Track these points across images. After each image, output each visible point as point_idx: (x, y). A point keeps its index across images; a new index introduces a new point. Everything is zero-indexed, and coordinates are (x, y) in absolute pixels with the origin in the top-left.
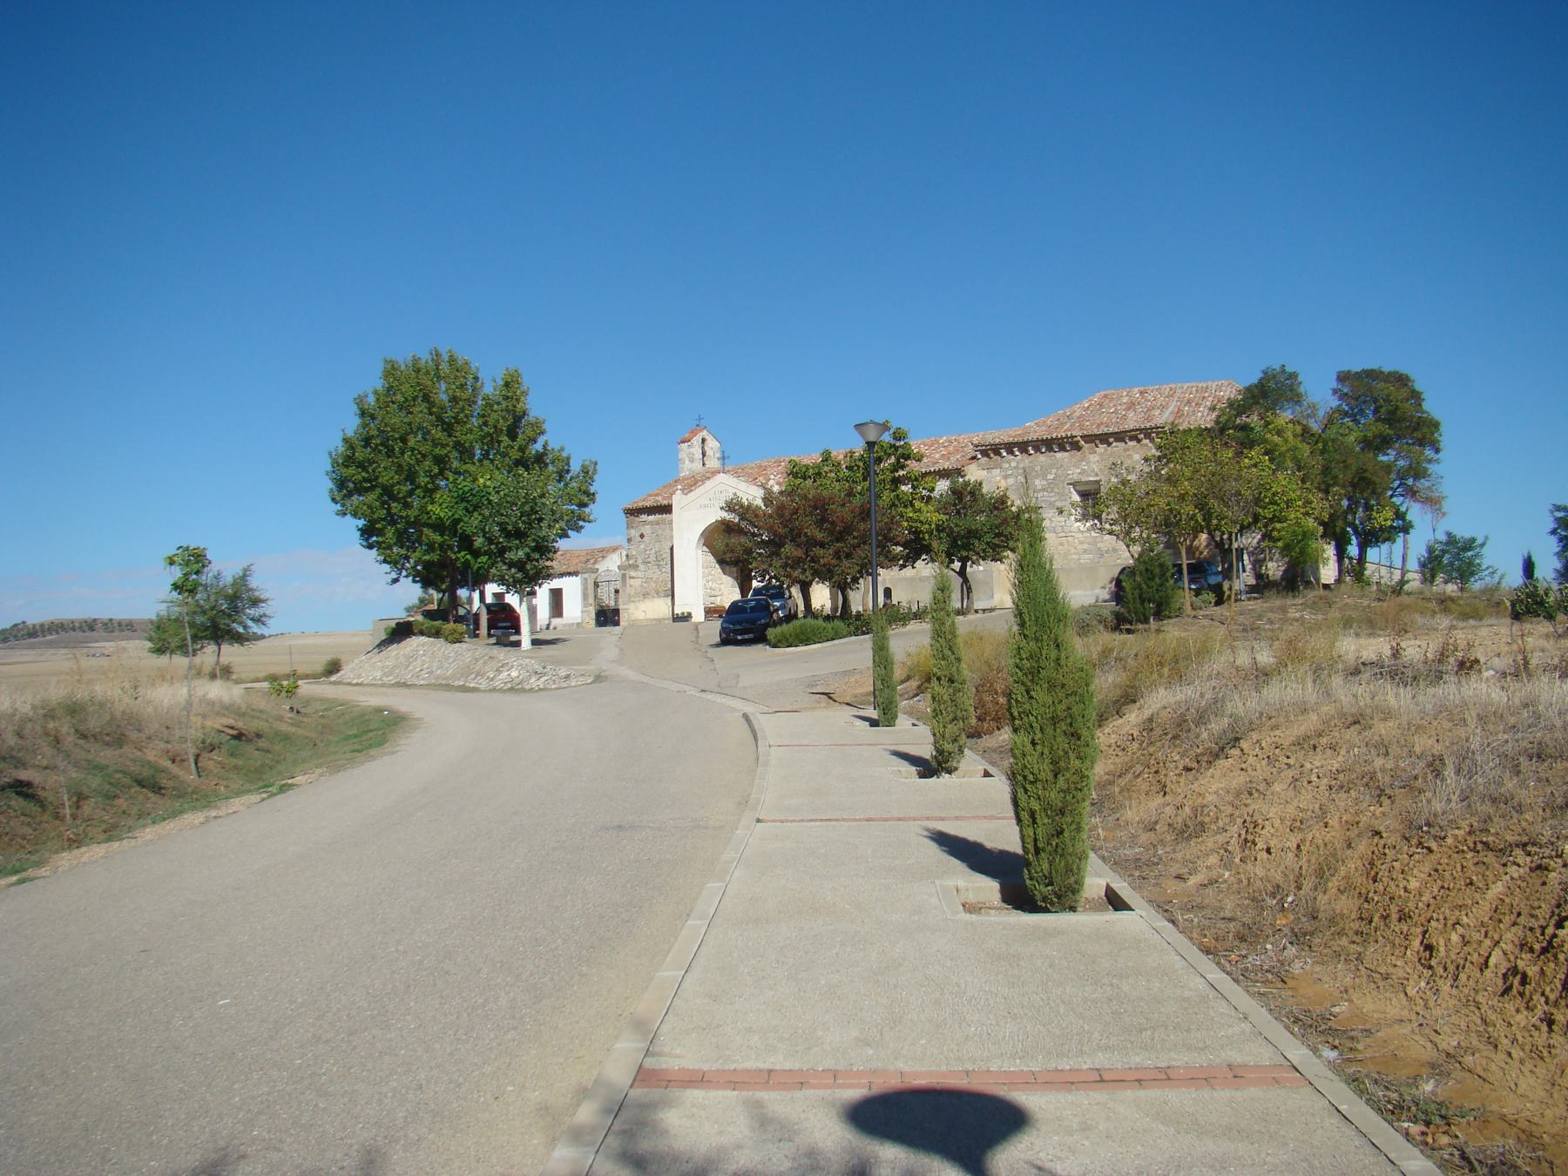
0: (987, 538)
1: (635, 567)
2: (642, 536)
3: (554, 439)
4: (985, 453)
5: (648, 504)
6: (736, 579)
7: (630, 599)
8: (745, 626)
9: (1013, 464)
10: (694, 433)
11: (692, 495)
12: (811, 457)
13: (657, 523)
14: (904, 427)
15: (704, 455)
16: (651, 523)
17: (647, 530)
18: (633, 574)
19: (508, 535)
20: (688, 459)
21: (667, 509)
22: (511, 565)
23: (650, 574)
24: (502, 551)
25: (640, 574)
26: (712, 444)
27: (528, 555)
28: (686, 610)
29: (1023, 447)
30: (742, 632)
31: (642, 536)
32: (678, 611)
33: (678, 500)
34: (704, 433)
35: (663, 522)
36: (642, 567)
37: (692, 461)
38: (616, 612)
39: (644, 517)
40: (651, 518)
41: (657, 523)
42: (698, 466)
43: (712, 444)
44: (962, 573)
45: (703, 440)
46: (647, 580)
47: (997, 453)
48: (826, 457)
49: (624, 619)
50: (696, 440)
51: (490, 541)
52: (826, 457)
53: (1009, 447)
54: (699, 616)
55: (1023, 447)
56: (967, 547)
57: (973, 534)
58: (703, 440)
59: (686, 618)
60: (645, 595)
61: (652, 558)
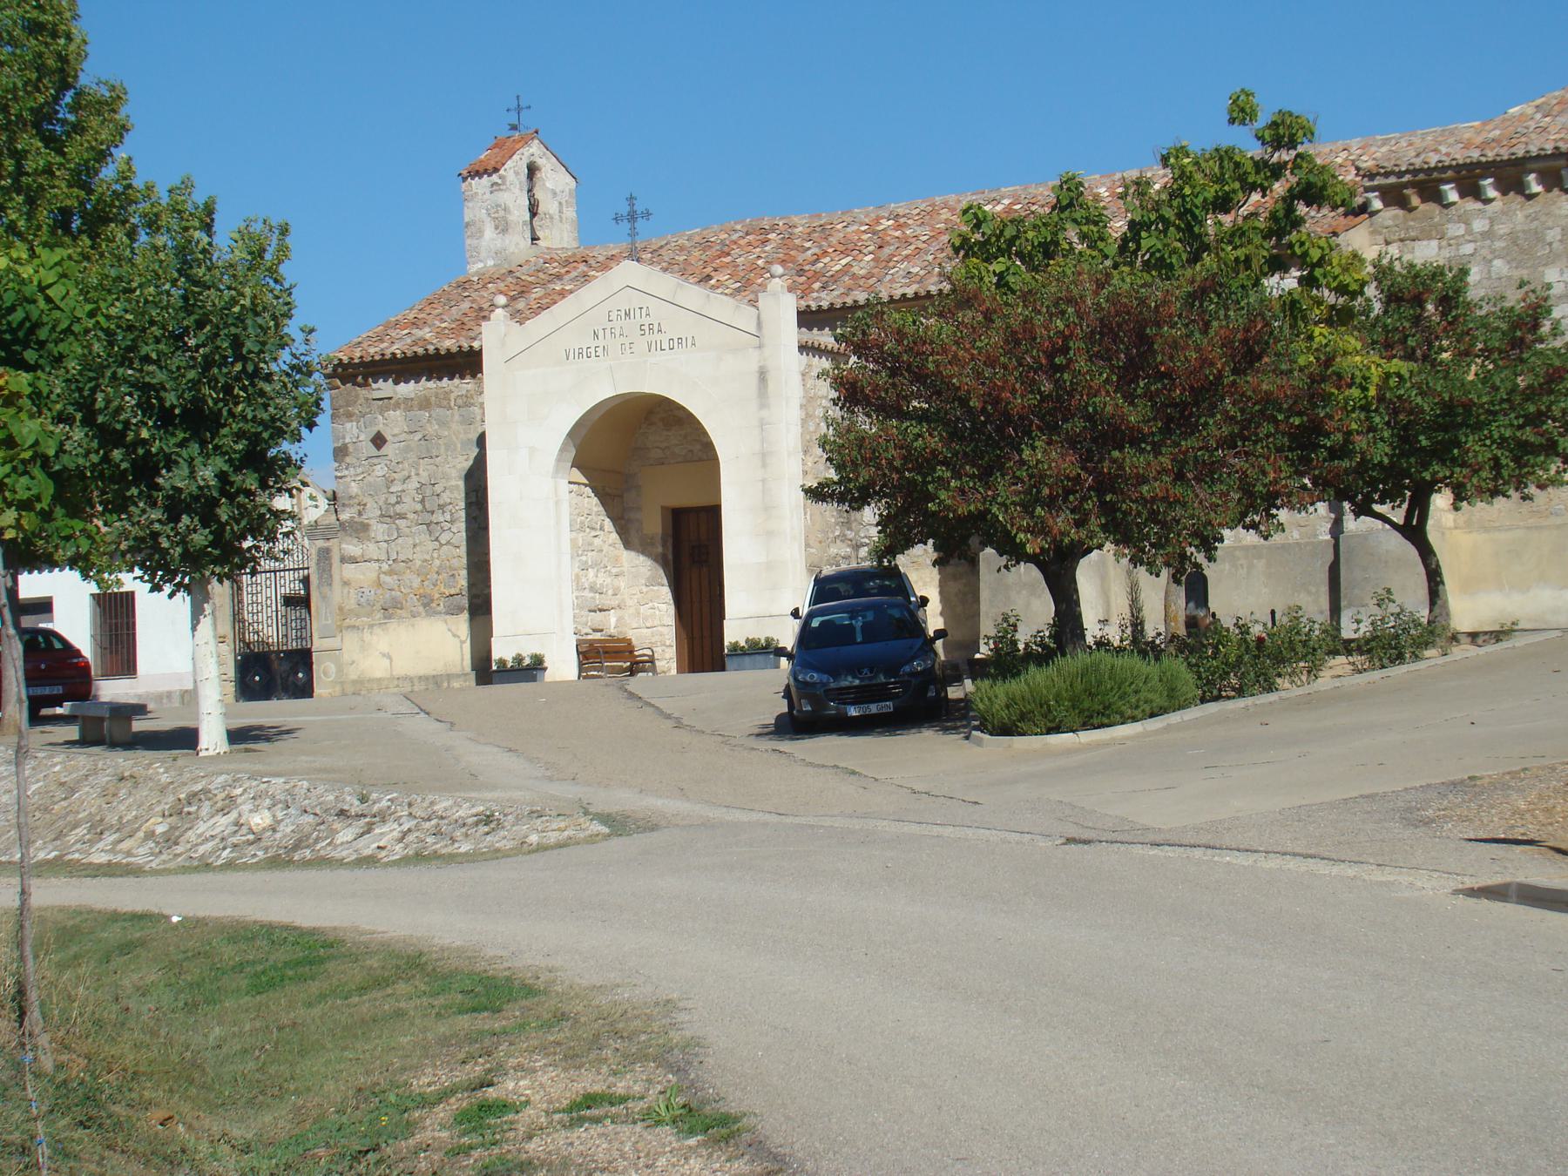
0: (1502, 427)
1: (359, 530)
2: (379, 441)
3: (154, 155)
4: (1394, 197)
5: (397, 349)
6: (662, 561)
7: (345, 621)
8: (866, 672)
9: (1479, 225)
10: (504, 148)
11: (539, 325)
12: (1019, 194)
13: (425, 404)
14: (1298, 106)
15: (533, 212)
16: (407, 405)
17: (393, 423)
18: (352, 548)
19: (165, 419)
20: (492, 227)
21: (467, 363)
22: (175, 507)
23: (403, 549)
24: (147, 469)
25: (372, 550)
26: (555, 180)
27: (222, 477)
28: (527, 651)
29: (1509, 175)
30: (862, 695)
31: (379, 441)
32: (503, 650)
33: (496, 338)
34: (534, 150)
35: (443, 400)
36: (379, 530)
37: (503, 227)
38: (303, 658)
39: (384, 387)
40: (407, 389)
41: (425, 404)
42: (517, 244)
43: (555, 180)
44: (1414, 532)
45: (532, 170)
46: (396, 565)
47: (1431, 193)
48: (1070, 199)
49: (324, 674)
50: (513, 171)
51: (109, 437)
52: (1070, 199)
53: (1469, 178)
54: (563, 666)
55: (1509, 175)
56: (1441, 453)
57: (1456, 417)
58: (532, 170)
59: (529, 670)
60: (390, 609)
61: (410, 505)
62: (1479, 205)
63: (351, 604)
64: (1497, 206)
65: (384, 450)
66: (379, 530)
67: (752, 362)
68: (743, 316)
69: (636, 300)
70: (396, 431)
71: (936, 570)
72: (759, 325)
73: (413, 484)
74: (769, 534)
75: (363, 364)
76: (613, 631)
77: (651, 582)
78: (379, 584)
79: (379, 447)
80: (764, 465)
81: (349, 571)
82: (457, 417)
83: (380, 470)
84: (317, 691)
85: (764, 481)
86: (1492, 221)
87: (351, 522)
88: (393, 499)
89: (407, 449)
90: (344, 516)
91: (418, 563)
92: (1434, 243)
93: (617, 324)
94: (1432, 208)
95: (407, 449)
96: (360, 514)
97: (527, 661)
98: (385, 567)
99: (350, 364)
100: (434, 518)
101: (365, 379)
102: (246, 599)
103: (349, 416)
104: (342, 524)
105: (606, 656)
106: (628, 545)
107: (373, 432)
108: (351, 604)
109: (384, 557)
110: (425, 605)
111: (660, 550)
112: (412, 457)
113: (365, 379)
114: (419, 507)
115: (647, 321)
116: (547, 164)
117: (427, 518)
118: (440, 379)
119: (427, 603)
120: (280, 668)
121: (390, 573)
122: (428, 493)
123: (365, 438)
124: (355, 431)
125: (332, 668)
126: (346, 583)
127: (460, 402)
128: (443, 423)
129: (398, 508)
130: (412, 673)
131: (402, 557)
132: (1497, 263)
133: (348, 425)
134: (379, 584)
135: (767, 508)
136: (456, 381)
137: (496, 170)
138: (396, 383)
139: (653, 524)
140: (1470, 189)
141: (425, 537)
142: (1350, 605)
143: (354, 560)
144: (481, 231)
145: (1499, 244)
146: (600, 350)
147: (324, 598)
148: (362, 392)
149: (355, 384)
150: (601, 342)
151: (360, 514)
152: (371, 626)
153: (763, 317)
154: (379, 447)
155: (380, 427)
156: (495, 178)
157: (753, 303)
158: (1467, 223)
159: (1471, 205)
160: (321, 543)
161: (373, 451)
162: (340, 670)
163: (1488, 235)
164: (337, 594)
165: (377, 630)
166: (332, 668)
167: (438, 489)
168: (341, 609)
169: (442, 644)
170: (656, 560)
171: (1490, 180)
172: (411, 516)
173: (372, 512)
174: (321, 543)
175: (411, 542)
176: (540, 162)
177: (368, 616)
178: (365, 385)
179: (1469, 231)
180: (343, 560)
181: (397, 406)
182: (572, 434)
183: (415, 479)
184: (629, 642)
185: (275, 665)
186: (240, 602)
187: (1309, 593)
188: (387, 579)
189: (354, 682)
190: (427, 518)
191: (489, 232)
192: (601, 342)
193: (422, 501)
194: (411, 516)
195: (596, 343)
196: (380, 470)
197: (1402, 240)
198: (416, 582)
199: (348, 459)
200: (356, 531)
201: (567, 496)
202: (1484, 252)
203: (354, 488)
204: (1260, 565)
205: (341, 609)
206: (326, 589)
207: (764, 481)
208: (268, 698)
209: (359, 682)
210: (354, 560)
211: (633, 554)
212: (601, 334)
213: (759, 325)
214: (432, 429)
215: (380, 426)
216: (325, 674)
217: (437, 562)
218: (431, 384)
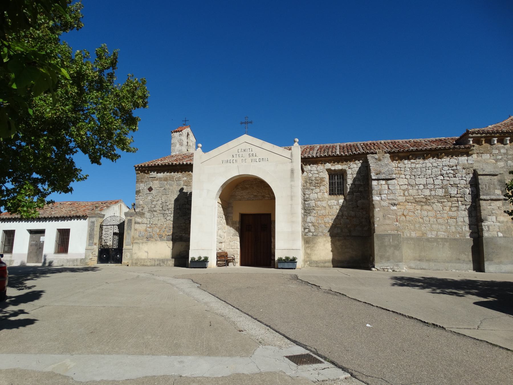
1: (141, 214)
9: (503, 151)
13: (166, 179)
16: (160, 179)
17: (155, 185)
18: (138, 220)
23: (155, 221)
25: (145, 221)
31: (150, 189)
35: (172, 179)
36: (148, 215)
37: (181, 144)
39: (154, 174)
40: (161, 175)
41: (166, 179)
45: (188, 135)
46: (152, 226)
47: (489, 141)
58: (188, 135)
60: (149, 238)
61: (158, 208)
62: (502, 145)
63: (137, 236)
64: (508, 146)
65: (151, 192)
66: (148, 215)
67: (289, 167)
68: (286, 153)
69: (248, 146)
70: (156, 187)
71: (170, 243)
72: (292, 155)
73: (160, 202)
74: (293, 222)
75: (148, 167)
76: (223, 249)
77: (234, 235)
78: (146, 231)
79: (150, 191)
80: (292, 200)
81: (137, 226)
82: (175, 183)
83: (150, 198)
84: (123, 261)
85: (291, 205)
86: (507, 150)
87: (139, 212)
88: (153, 206)
89: (159, 192)
90: (137, 210)
91: (159, 225)
92: (488, 155)
93: (241, 153)
94: (488, 145)
95: (159, 192)
96: (142, 210)
97: (203, 259)
98: (148, 226)
99: (145, 167)
100: (165, 212)
101: (148, 171)
102: (104, 232)
103: (142, 182)
104: (136, 213)
105: (224, 259)
106: (228, 224)
107: (149, 186)
108: (137, 236)
109: (148, 223)
110: (160, 238)
111: (238, 226)
112: (160, 194)
113: (148, 171)
114: (161, 209)
115: (251, 153)
116: (191, 134)
117: (163, 212)
118: (171, 173)
119: (161, 237)
120: (112, 253)
121: (150, 228)
122: (164, 204)
123: (146, 188)
124: (143, 186)
125: (129, 254)
126: (136, 230)
127: (177, 179)
128: (171, 185)
129: (154, 209)
130: (154, 257)
131: (154, 223)
132: (509, 162)
133: (141, 184)
134: (146, 231)
135: (293, 213)
136: (176, 173)
137: (181, 131)
138: (157, 173)
139: (237, 218)
140: (501, 141)
141: (162, 218)
142: (487, 260)
143: (139, 223)
144: (176, 146)
145: (509, 157)
146: (234, 161)
147: (128, 234)
148: (147, 175)
149: (145, 173)
150: (235, 159)
151: (142, 210)
152: (142, 243)
153: (293, 153)
154: (150, 191)
155: (151, 185)
156: (181, 133)
157: (290, 149)
158: (499, 150)
159: (500, 145)
160: (129, 218)
161: (148, 192)
162: (131, 255)
163: (506, 154)
164: (132, 233)
165: (144, 244)
166: (129, 254)
167: (168, 204)
168: (133, 237)
169: (165, 249)
170: (236, 229)
171: (509, 138)
172: (158, 211)
173: (146, 209)
174: (129, 218)
175: (157, 219)
176: (190, 133)
177: (142, 240)
178: (148, 173)
179: (500, 152)
180: (135, 223)
181: (157, 180)
182: (222, 186)
183: (160, 201)
184: (226, 253)
185: (111, 252)
186: (102, 233)
187: (465, 255)
188: (149, 229)
189: (136, 260)
190: (163, 212)
191: (178, 145)
192: (235, 159)
193: (162, 207)
194: (158, 211)
195: (233, 159)
196: (150, 198)
197: (477, 153)
198: (158, 231)
199: (140, 194)
200: (141, 215)
201: (217, 206)
202: (505, 158)
203: (141, 202)
204: (447, 244)
205: (133, 237)
206: (129, 231)
207: (291, 205)
208: (107, 262)
209: (138, 259)
210: (139, 223)
211: (229, 227)
212: (235, 156)
213: (292, 155)
214: (167, 187)
215: (151, 185)
216: (126, 256)
217: (165, 225)
218: (168, 174)
